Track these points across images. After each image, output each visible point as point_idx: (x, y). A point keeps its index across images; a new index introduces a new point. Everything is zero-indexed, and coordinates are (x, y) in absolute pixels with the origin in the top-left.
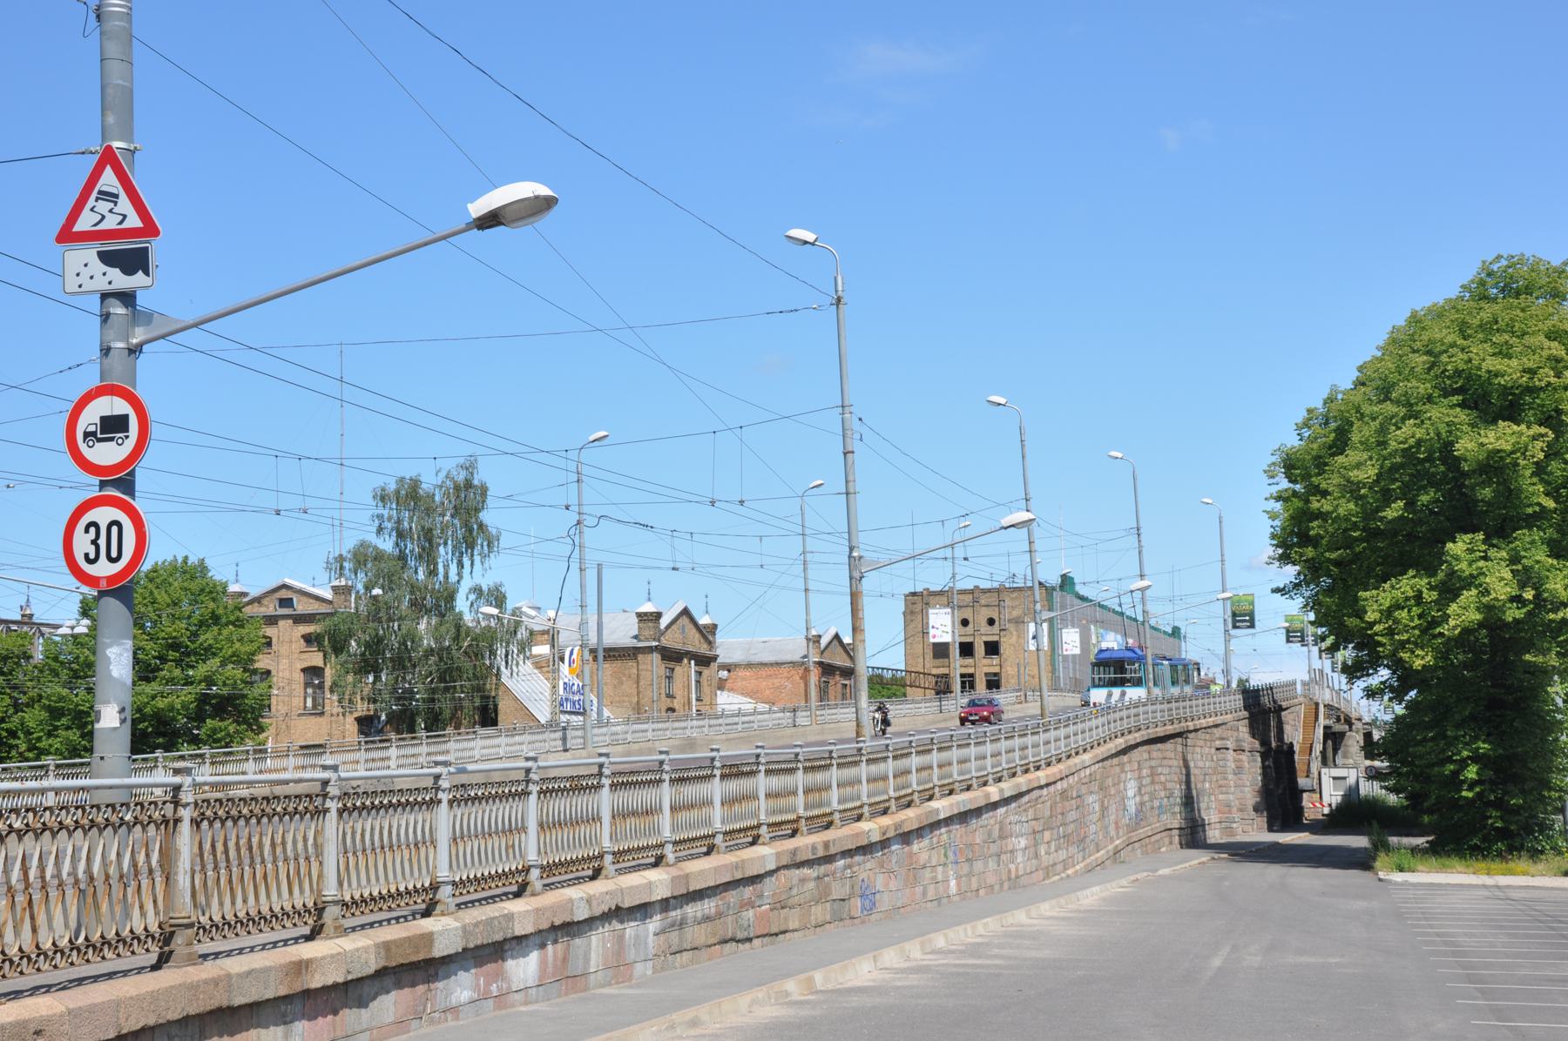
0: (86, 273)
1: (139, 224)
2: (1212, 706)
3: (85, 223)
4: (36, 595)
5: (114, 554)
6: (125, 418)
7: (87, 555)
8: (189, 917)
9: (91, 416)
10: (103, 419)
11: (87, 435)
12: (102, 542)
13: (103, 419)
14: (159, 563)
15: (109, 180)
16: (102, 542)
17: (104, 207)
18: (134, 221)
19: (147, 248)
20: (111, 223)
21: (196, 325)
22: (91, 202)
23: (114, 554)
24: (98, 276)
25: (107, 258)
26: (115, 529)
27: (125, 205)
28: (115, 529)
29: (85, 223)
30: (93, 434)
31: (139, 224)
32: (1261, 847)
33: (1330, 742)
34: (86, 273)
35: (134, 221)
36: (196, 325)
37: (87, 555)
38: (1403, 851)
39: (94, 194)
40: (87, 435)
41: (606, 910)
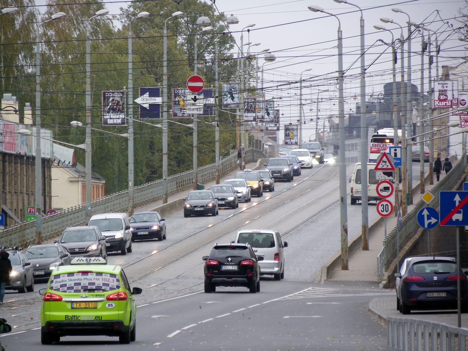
0: (380, 176)
3: (380, 166)
4: (244, 43)
5: (387, 210)
6: (389, 187)
7: (382, 210)
10: (384, 187)
11: (381, 190)
13: (384, 187)
15: (385, 159)
17: (384, 164)
18: (390, 167)
19: (392, 173)
20: (385, 167)
21: (372, 64)
22: (381, 163)
23: (387, 210)
24: (383, 177)
25: (384, 173)
26: (387, 206)
27: (388, 163)
28: (387, 206)
29: (380, 166)
30: (382, 190)
32: (421, 255)
34: (380, 176)
35: (390, 167)
36: (372, 64)
37: (382, 210)
39: (382, 161)
40: (381, 190)
41: (392, 263)
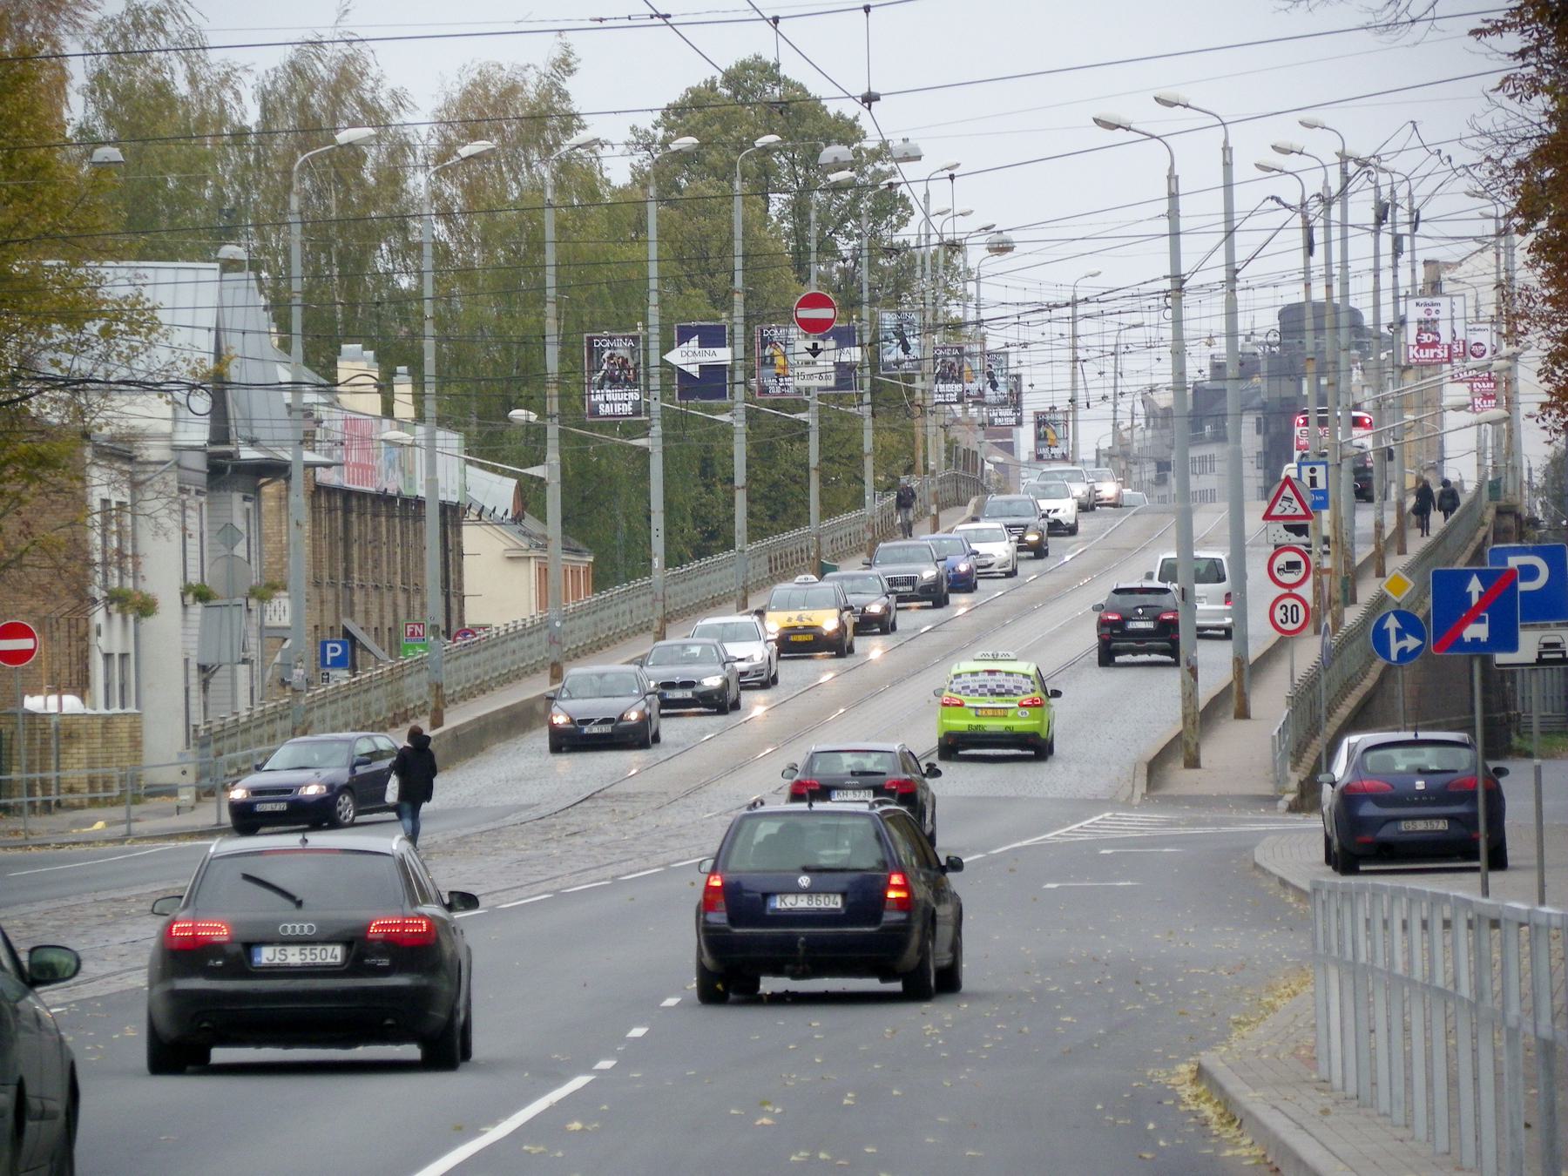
0: (1278, 534)
1: (1304, 513)
2: (628, 616)
3: (1276, 511)
8: (201, 505)
9: (1282, 560)
11: (1279, 570)
12: (1289, 614)
14: (971, 287)
15: (1288, 491)
16: (1289, 614)
17: (1285, 504)
18: (1301, 512)
20: (1289, 512)
22: (1280, 501)
27: (1296, 503)
29: (1276, 511)
31: (1304, 513)
33: (1118, 659)
34: (1278, 534)
35: (1301, 512)
38: (201, 232)
40: (1279, 570)
